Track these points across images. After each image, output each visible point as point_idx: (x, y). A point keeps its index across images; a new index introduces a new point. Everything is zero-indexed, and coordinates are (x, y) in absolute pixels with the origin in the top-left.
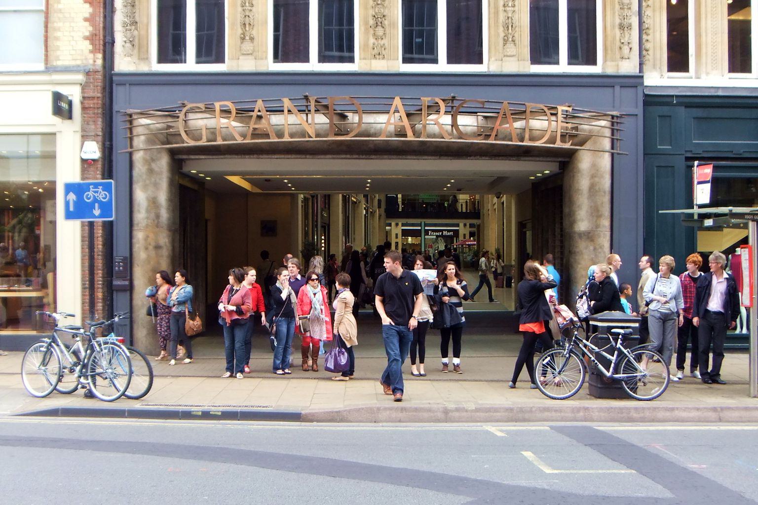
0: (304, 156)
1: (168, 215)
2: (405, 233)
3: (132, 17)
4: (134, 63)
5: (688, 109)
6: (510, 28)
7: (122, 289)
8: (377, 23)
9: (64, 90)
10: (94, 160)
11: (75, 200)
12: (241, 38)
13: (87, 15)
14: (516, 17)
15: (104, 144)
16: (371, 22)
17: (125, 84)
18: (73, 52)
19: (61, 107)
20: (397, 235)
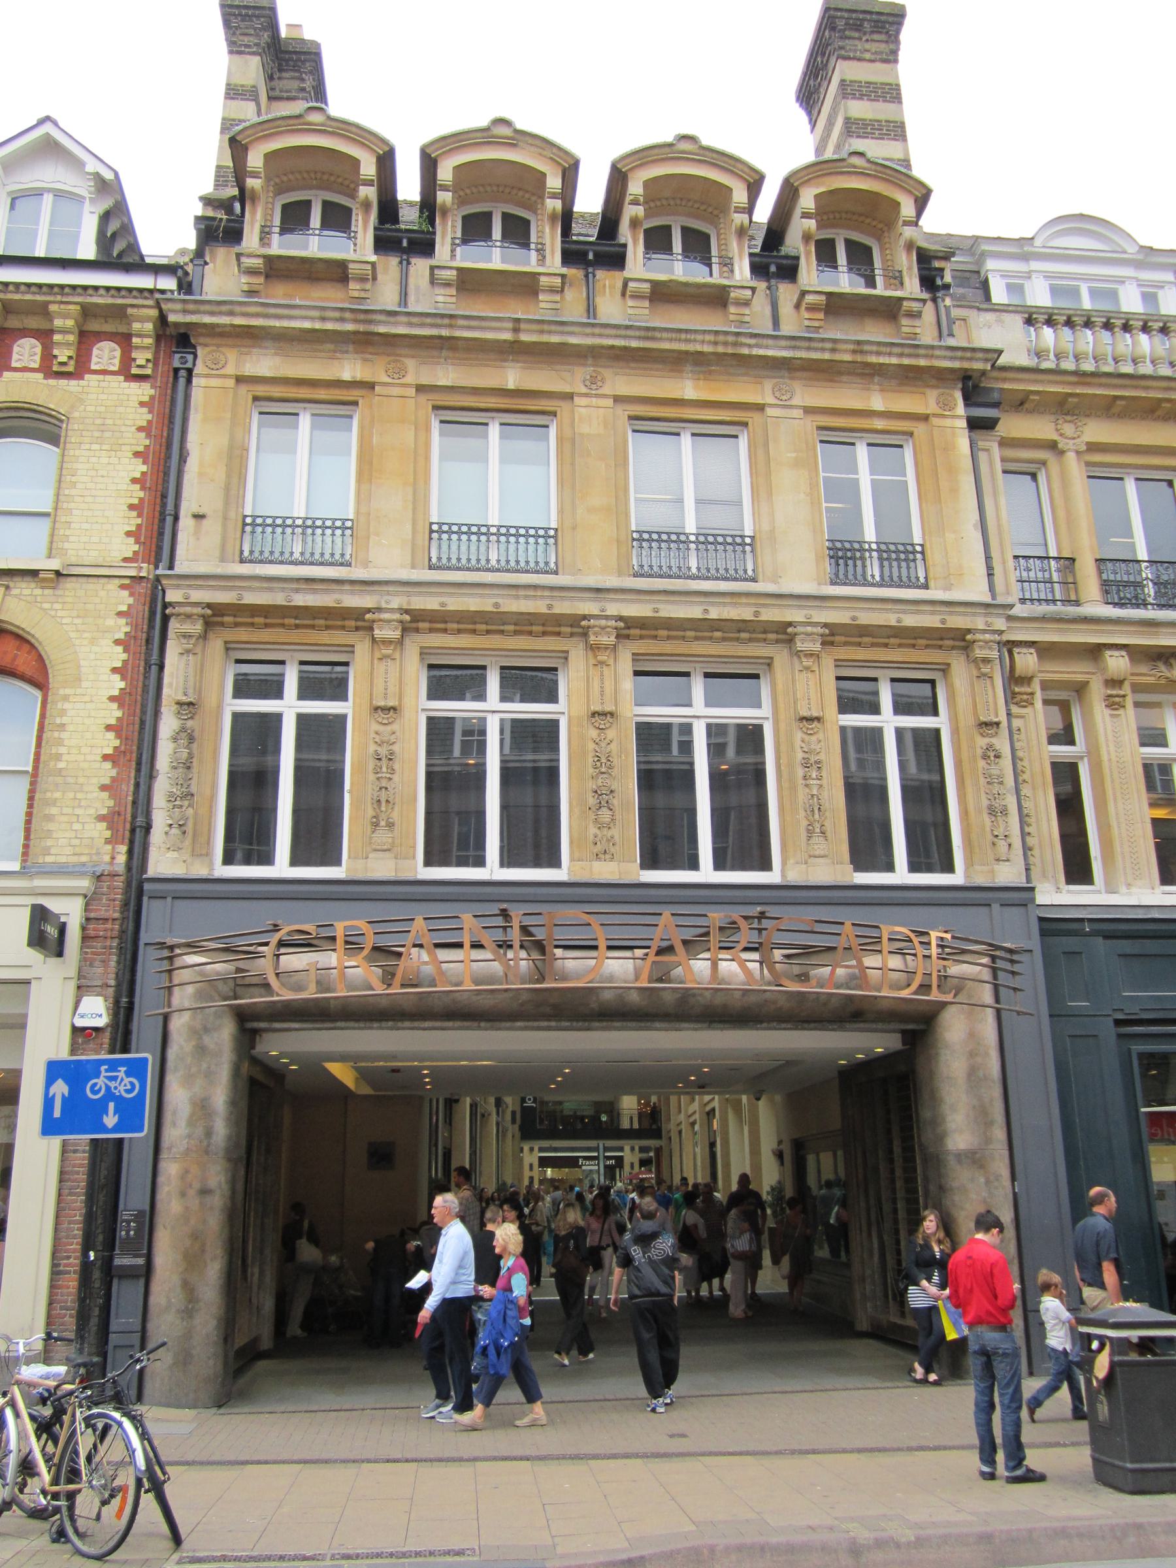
0: (475, 1024)
2: (544, 1162)
5: (1109, 942)
6: (816, 811)
7: (129, 1274)
10: (96, 1029)
11: (67, 1095)
12: (372, 823)
14: (825, 794)
15: (117, 1002)
16: (592, 801)
18: (77, 842)
19: (45, 934)
20: (531, 1166)
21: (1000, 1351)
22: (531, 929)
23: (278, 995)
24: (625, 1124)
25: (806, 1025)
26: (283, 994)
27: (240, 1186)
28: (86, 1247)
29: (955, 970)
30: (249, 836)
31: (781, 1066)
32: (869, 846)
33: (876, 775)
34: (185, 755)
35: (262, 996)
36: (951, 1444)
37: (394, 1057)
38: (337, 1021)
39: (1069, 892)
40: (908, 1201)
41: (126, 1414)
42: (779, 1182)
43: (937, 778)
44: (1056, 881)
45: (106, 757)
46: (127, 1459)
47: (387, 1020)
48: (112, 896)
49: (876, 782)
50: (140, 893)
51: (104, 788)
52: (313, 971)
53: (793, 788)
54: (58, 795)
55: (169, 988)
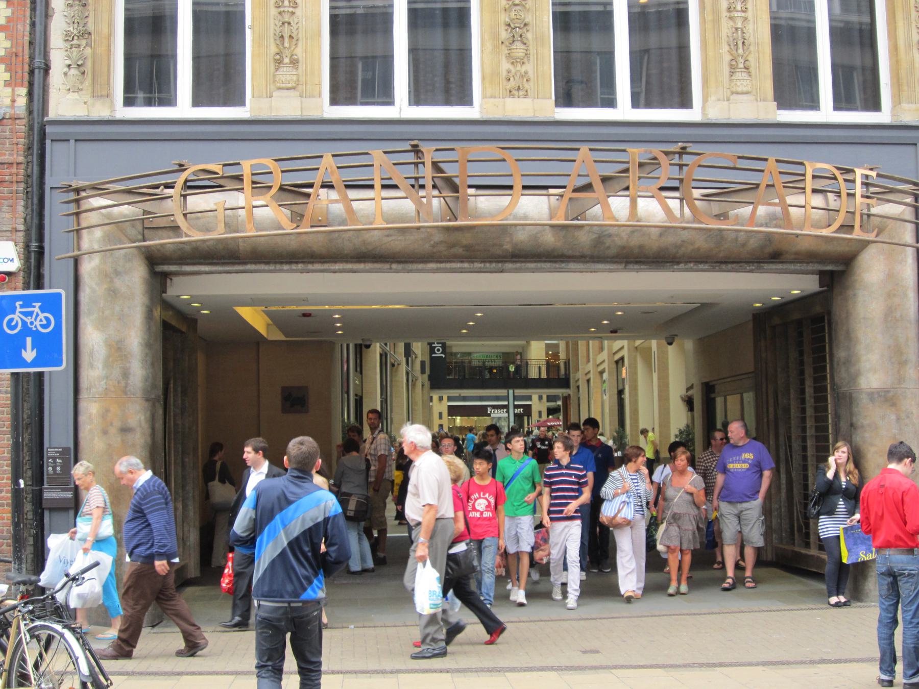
0: (387, 266)
1: (144, 373)
2: (453, 411)
3: (82, 25)
4: (85, 103)
6: (740, 45)
8: (513, 36)
10: (9, 274)
14: (750, 28)
15: (27, 247)
16: (504, 35)
17: (68, 140)
20: (441, 414)
21: (906, 572)
22: (441, 165)
23: (187, 235)
24: (533, 374)
25: (724, 267)
26: (193, 235)
27: (159, 425)
28: (16, 475)
29: (879, 209)
30: (148, 76)
31: (698, 308)
32: (794, 83)
33: (804, 17)
36: (852, 657)
37: (305, 301)
38: (245, 263)
40: (818, 439)
41: (65, 627)
42: (688, 426)
43: (866, 19)
46: (71, 668)
47: (297, 263)
48: (15, 140)
49: (804, 24)
50: (43, 136)
52: (221, 210)
53: (717, 21)
55: (78, 231)
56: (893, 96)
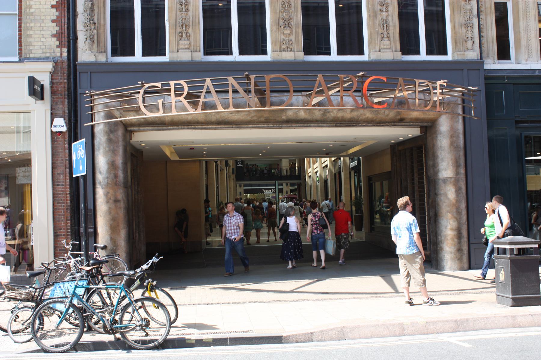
2: (246, 191)
9: (38, 77)
13: (55, 18)
15: (70, 120)
16: (281, 22)
18: (44, 47)
19: (35, 90)
20: (240, 193)
23: (145, 115)
24: (284, 173)
30: (122, 43)
32: (409, 44)
34: (90, 5)
35: (134, 116)
39: (498, 63)
44: (494, 59)
45: (53, 6)
51: (53, 21)
54: (32, 25)
56: (453, 49)
